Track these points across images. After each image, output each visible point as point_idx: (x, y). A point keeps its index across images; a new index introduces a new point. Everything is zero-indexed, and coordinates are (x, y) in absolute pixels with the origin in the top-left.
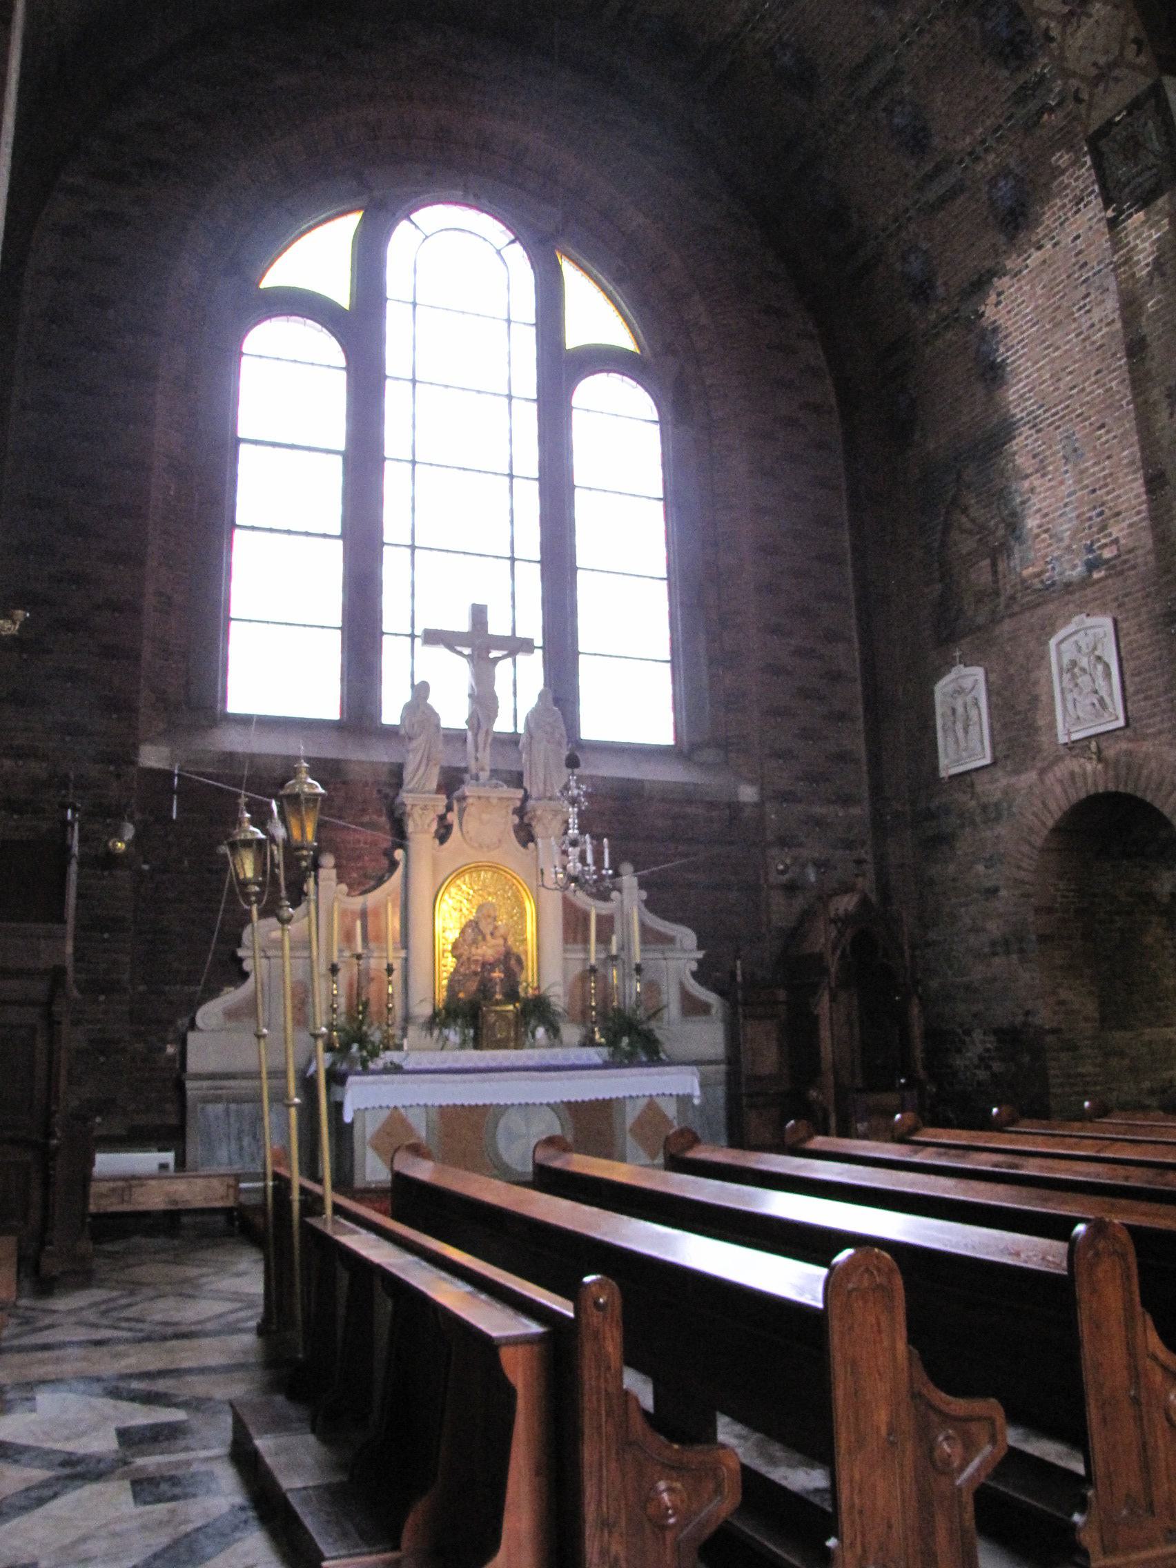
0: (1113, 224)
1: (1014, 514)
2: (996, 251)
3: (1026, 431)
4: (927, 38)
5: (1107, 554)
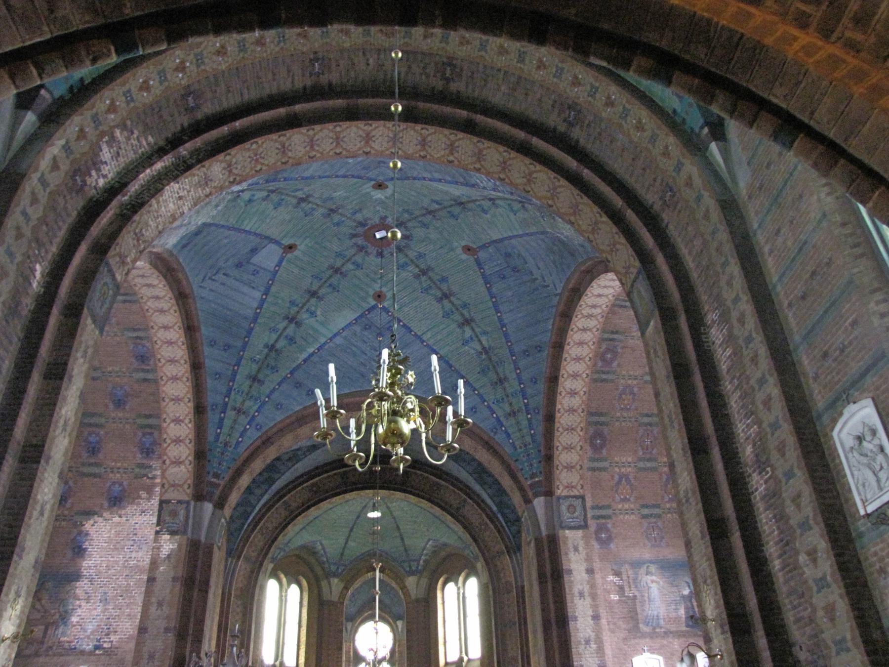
0: (157, 533)
1: (66, 612)
2: (102, 507)
3: (86, 581)
4: (121, 426)
5: (105, 645)
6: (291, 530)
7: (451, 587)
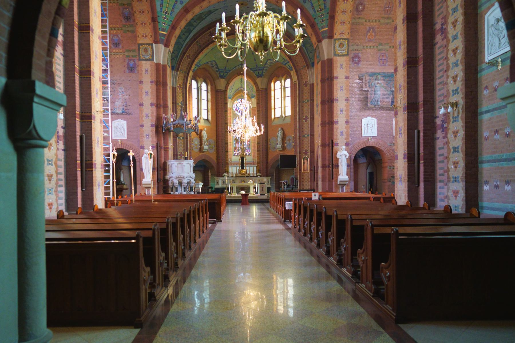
6: (201, 56)
7: (278, 83)
